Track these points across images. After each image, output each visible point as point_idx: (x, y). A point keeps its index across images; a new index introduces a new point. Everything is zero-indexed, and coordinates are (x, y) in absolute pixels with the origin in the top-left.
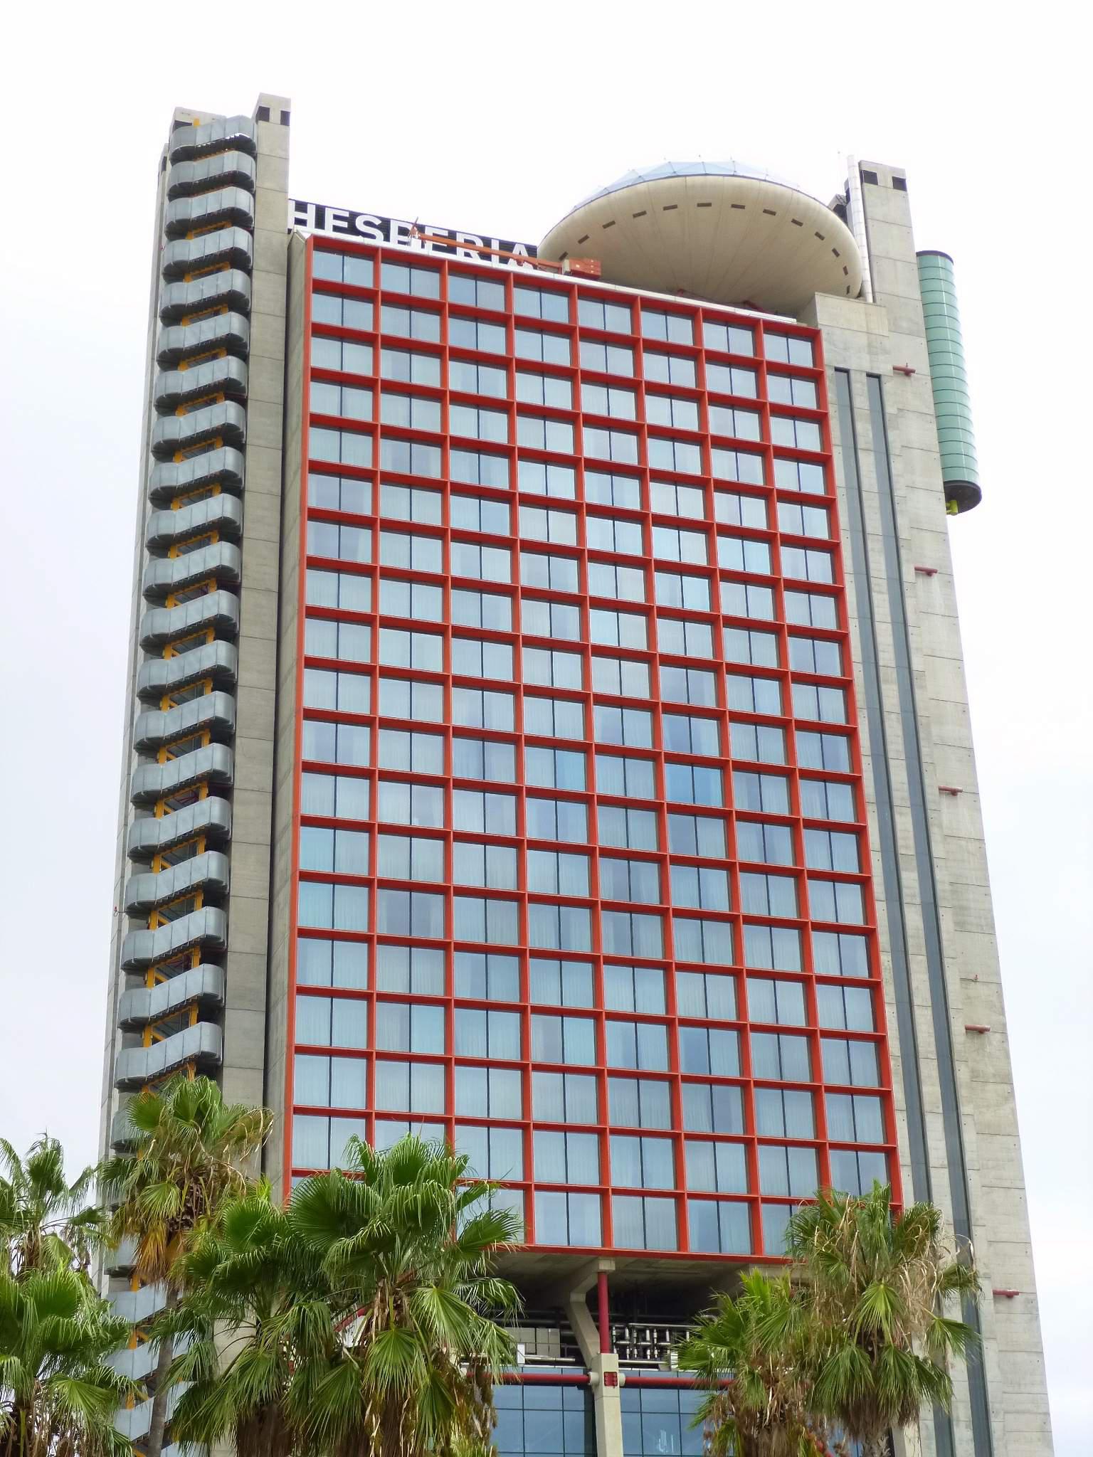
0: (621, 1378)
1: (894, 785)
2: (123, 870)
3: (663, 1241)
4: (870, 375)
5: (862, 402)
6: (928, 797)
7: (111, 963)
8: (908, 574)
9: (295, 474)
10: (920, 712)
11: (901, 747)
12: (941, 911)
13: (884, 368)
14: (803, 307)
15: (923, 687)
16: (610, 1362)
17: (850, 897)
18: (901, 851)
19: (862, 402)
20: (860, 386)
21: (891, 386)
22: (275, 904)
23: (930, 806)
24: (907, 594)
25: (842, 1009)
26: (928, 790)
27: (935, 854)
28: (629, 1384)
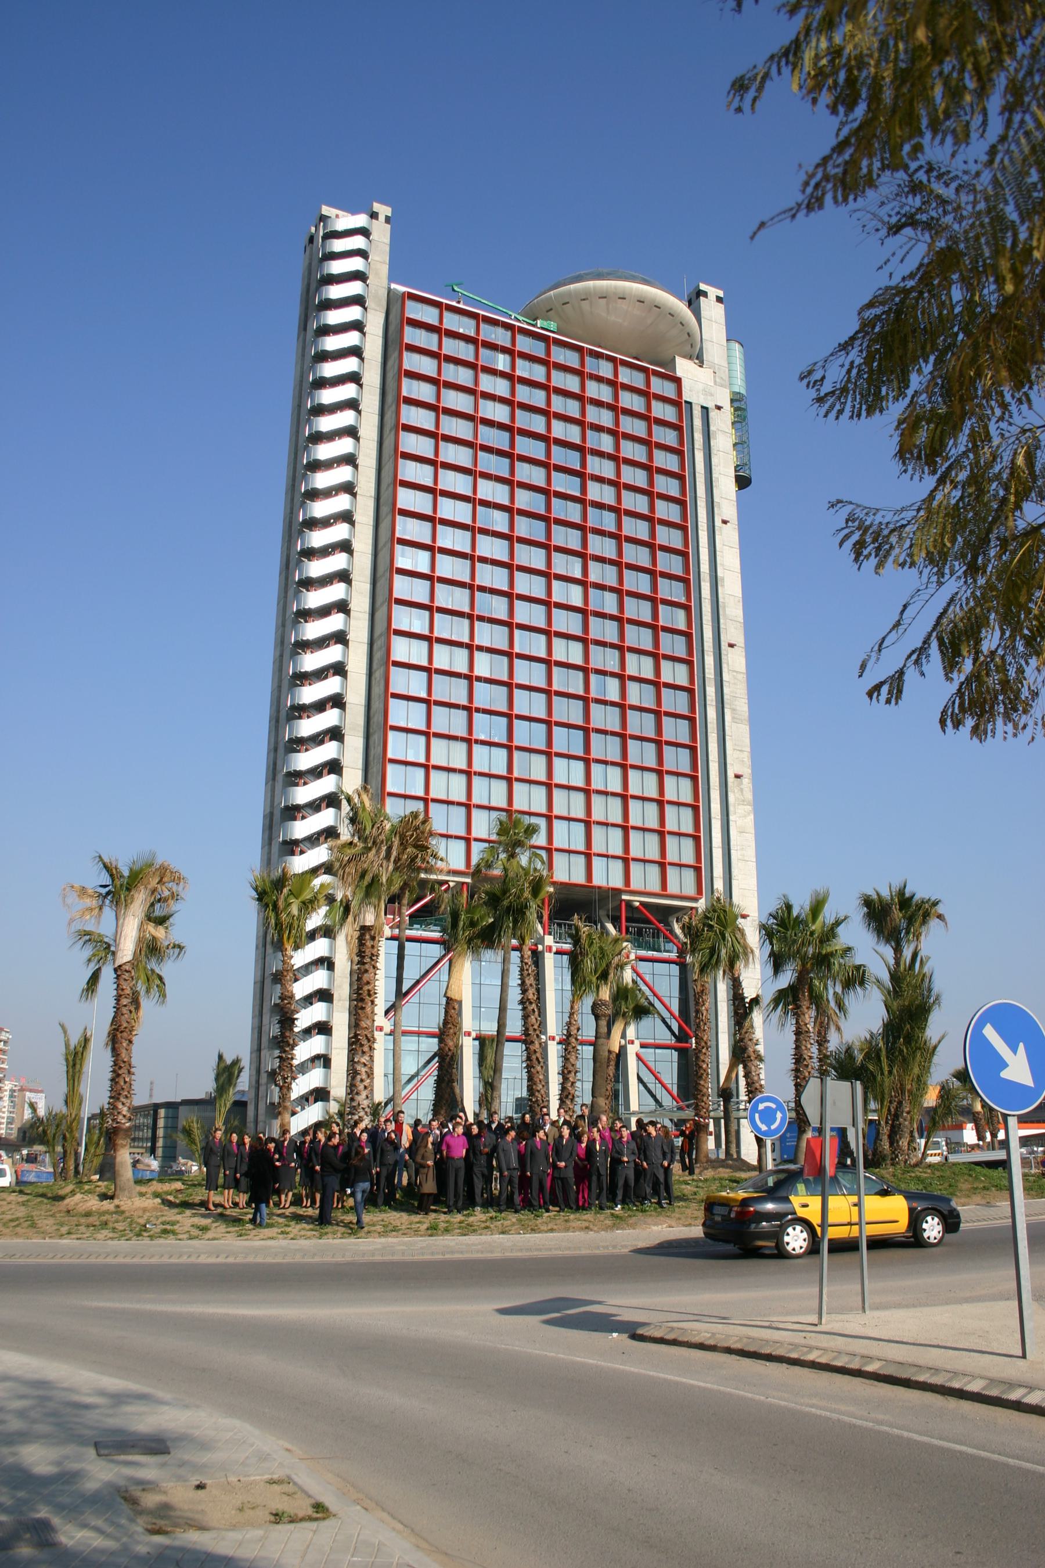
0: (554, 949)
1: (705, 639)
2: (269, 853)
3: (579, 877)
4: (702, 407)
5: (698, 423)
6: (723, 647)
7: (256, 961)
8: (718, 523)
9: (391, 430)
10: (721, 600)
11: (710, 618)
12: (726, 710)
13: (711, 405)
14: (671, 364)
15: (723, 586)
16: (549, 940)
17: (682, 670)
18: (707, 676)
19: (698, 423)
20: (697, 413)
21: (713, 414)
22: (370, 771)
23: (723, 652)
24: (717, 532)
25: (674, 673)
26: (723, 643)
27: (724, 679)
28: (558, 953)
